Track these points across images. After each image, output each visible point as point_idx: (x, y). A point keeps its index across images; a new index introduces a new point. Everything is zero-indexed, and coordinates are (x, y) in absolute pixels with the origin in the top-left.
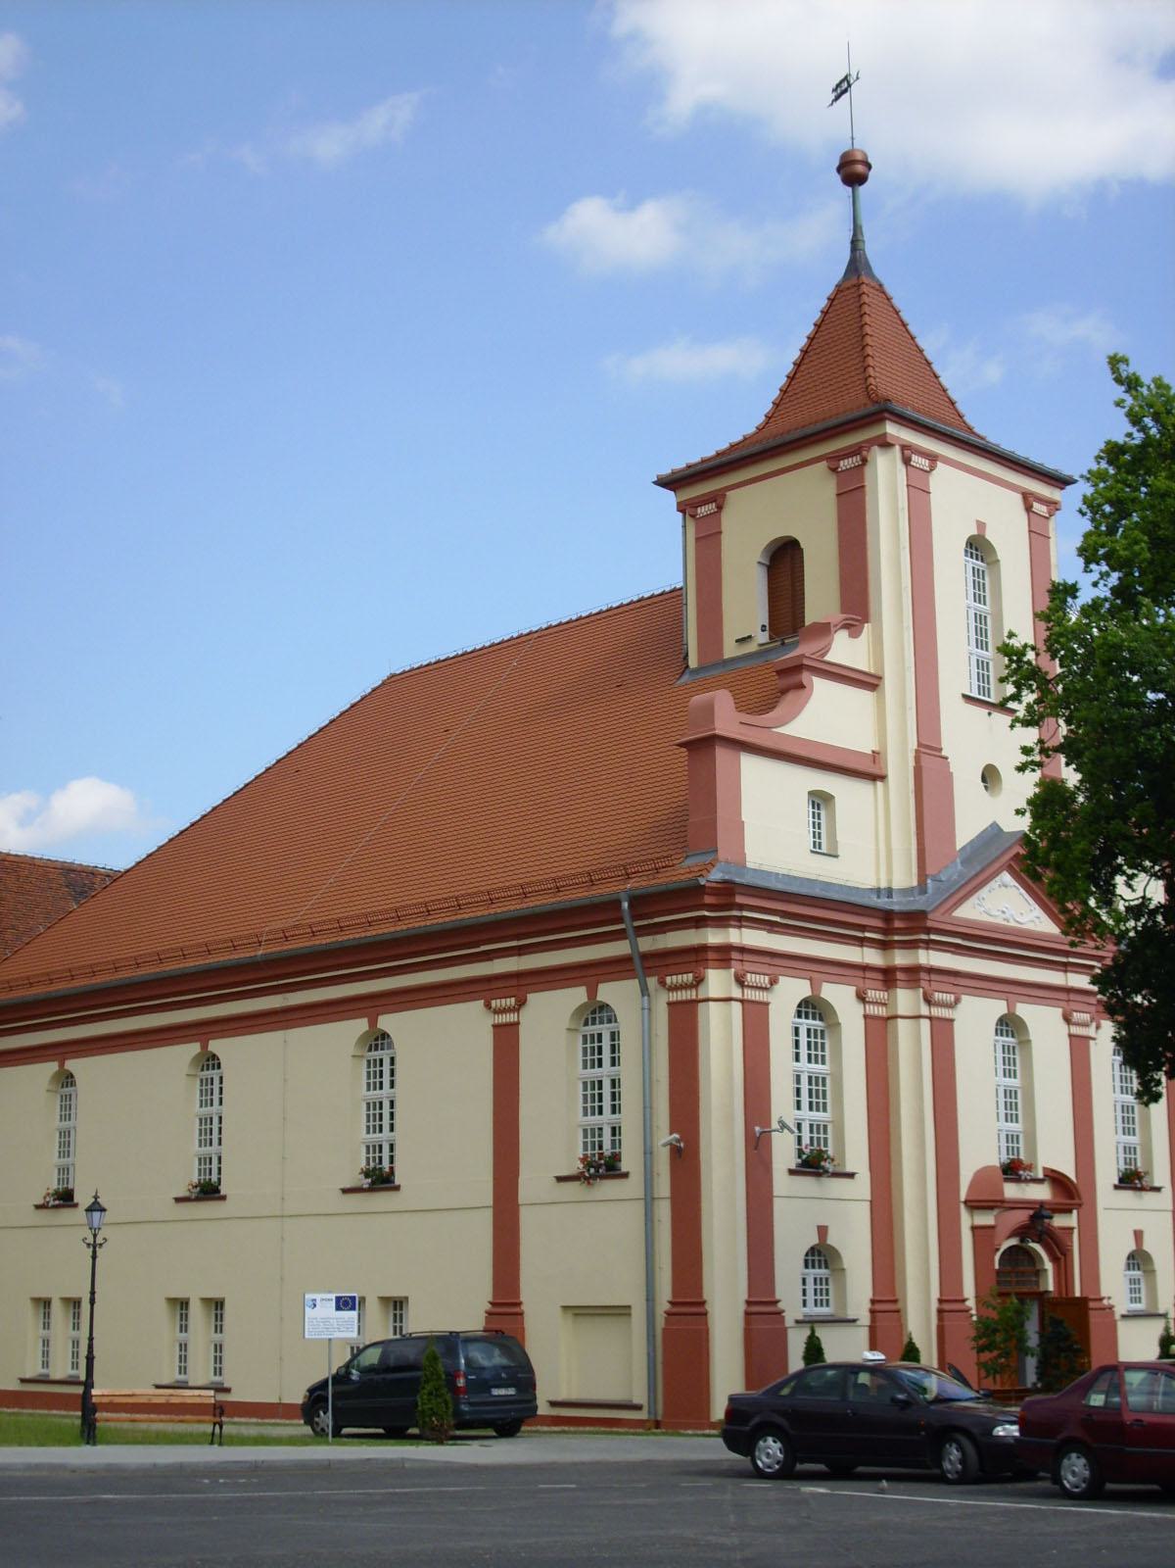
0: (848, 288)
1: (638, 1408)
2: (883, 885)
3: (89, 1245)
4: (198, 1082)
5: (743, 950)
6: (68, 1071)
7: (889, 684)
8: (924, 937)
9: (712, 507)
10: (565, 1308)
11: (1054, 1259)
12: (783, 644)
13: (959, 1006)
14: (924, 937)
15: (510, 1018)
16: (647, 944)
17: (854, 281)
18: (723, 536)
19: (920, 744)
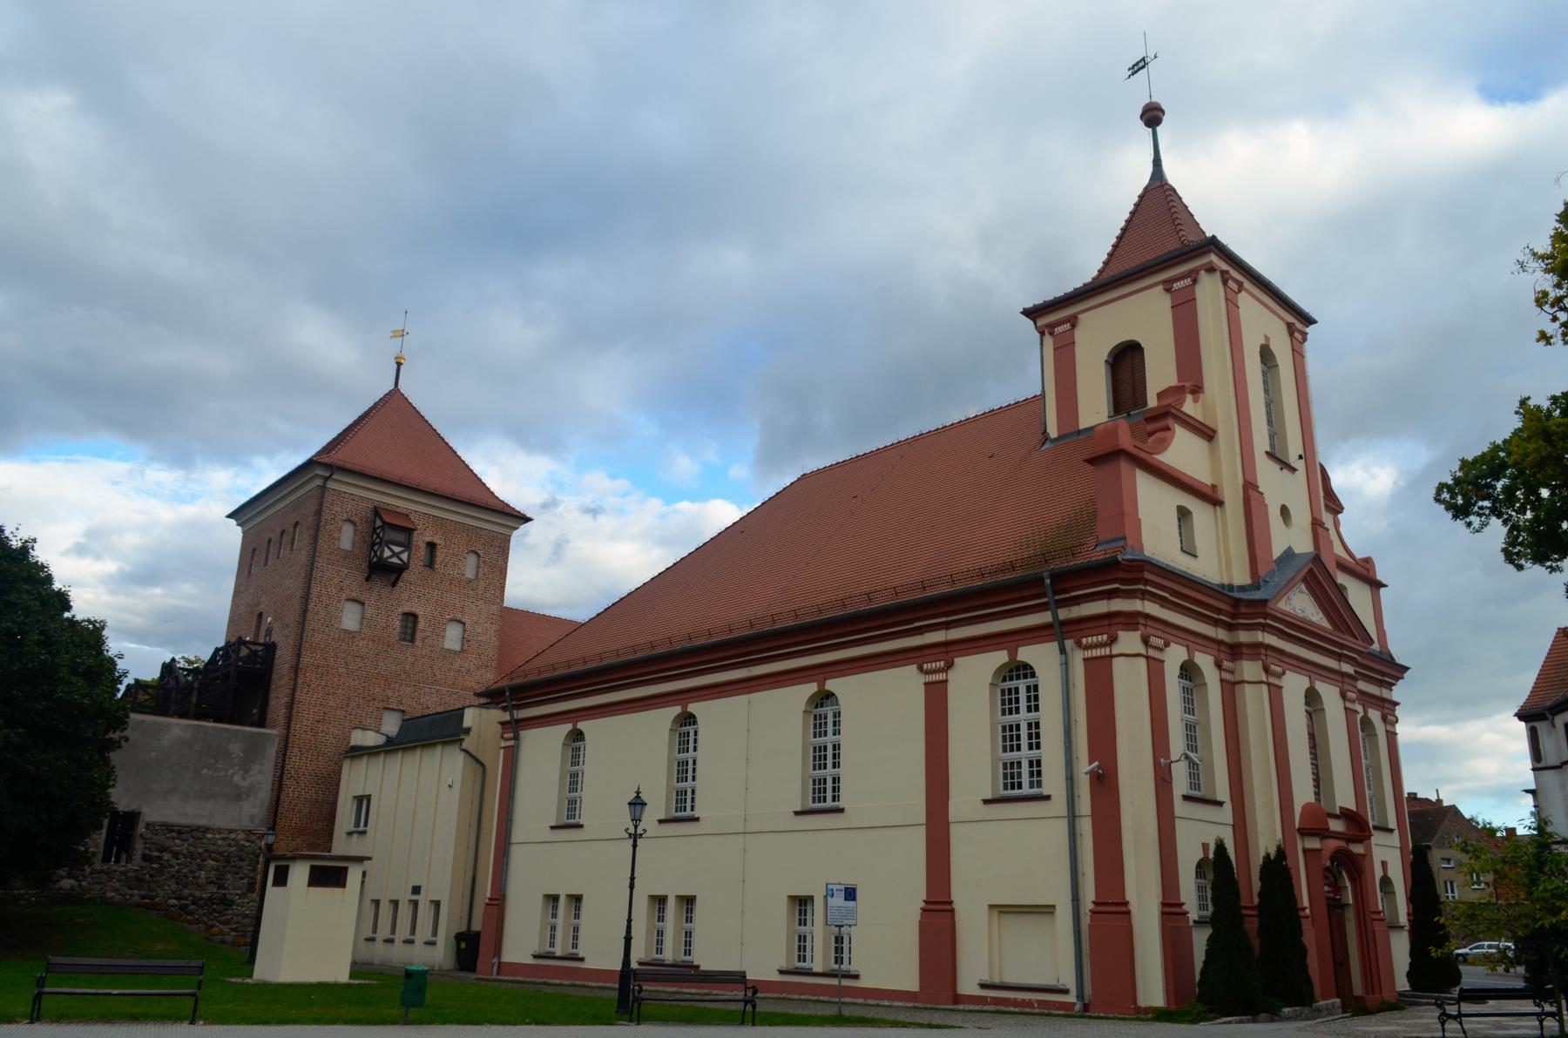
0: (1154, 189)
1: (1066, 992)
3: (630, 834)
4: (678, 735)
6: (579, 730)
8: (1262, 621)
9: (1067, 326)
10: (992, 907)
11: (1352, 879)
12: (1129, 415)
13: (1284, 677)
15: (941, 677)
16: (1064, 614)
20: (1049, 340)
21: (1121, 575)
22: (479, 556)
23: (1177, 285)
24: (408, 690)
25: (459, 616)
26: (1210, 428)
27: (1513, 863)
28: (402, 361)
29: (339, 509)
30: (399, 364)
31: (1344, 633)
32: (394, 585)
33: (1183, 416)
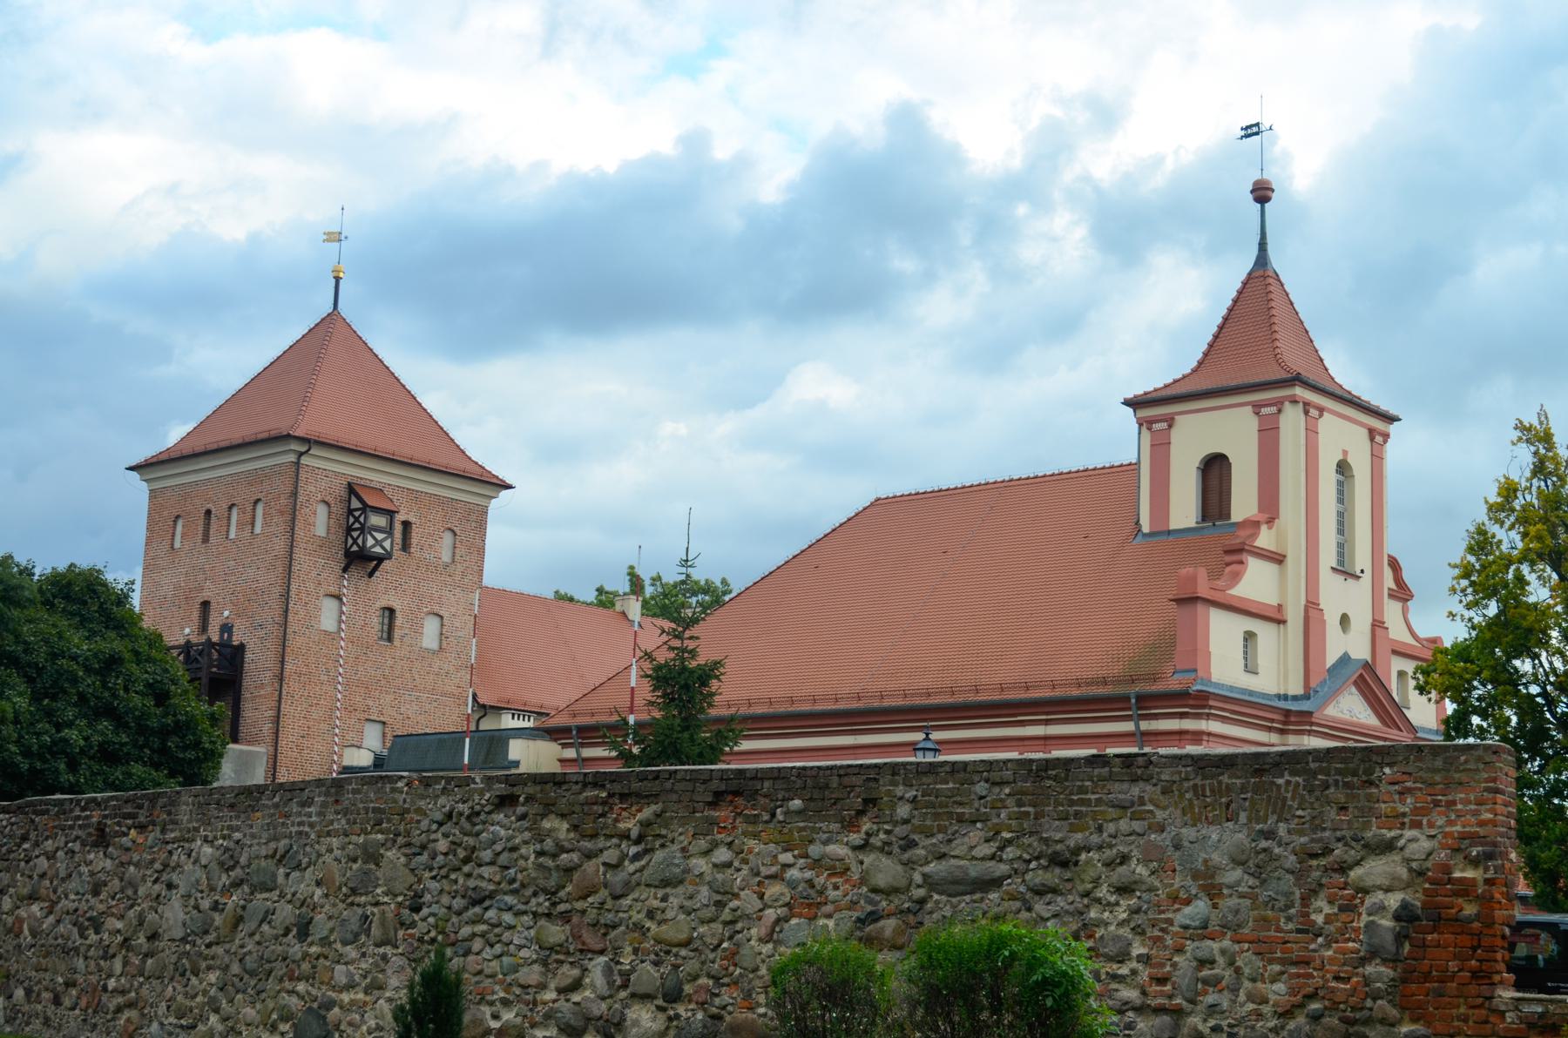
2: (1282, 692)
5: (1209, 734)
7: (1289, 560)
8: (1308, 728)
14: (1308, 728)
16: (1145, 725)
17: (1260, 273)
18: (1172, 446)
19: (1307, 601)
20: (1146, 435)
21: (1191, 702)
22: (455, 534)
23: (1265, 411)
24: (389, 698)
25: (436, 609)
26: (1280, 555)
27: (810, 963)
28: (341, 275)
29: (313, 489)
30: (337, 279)
31: (1390, 727)
32: (371, 575)
33: (1256, 550)
